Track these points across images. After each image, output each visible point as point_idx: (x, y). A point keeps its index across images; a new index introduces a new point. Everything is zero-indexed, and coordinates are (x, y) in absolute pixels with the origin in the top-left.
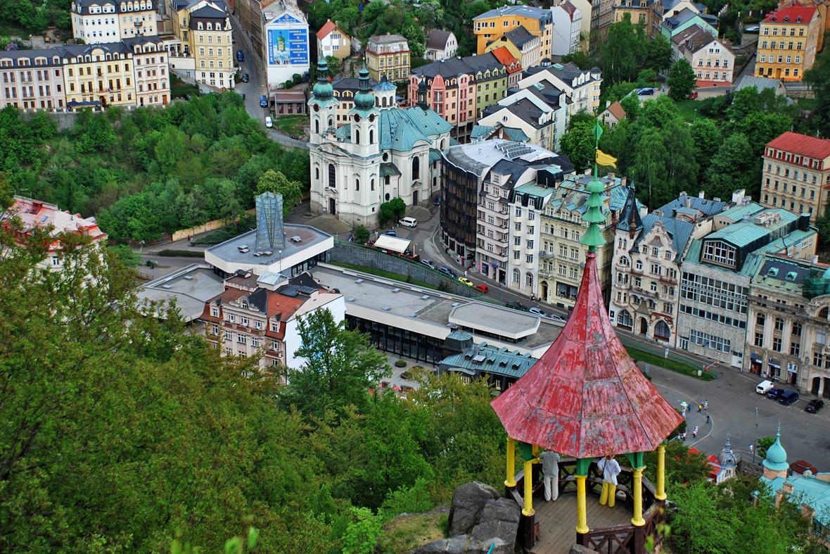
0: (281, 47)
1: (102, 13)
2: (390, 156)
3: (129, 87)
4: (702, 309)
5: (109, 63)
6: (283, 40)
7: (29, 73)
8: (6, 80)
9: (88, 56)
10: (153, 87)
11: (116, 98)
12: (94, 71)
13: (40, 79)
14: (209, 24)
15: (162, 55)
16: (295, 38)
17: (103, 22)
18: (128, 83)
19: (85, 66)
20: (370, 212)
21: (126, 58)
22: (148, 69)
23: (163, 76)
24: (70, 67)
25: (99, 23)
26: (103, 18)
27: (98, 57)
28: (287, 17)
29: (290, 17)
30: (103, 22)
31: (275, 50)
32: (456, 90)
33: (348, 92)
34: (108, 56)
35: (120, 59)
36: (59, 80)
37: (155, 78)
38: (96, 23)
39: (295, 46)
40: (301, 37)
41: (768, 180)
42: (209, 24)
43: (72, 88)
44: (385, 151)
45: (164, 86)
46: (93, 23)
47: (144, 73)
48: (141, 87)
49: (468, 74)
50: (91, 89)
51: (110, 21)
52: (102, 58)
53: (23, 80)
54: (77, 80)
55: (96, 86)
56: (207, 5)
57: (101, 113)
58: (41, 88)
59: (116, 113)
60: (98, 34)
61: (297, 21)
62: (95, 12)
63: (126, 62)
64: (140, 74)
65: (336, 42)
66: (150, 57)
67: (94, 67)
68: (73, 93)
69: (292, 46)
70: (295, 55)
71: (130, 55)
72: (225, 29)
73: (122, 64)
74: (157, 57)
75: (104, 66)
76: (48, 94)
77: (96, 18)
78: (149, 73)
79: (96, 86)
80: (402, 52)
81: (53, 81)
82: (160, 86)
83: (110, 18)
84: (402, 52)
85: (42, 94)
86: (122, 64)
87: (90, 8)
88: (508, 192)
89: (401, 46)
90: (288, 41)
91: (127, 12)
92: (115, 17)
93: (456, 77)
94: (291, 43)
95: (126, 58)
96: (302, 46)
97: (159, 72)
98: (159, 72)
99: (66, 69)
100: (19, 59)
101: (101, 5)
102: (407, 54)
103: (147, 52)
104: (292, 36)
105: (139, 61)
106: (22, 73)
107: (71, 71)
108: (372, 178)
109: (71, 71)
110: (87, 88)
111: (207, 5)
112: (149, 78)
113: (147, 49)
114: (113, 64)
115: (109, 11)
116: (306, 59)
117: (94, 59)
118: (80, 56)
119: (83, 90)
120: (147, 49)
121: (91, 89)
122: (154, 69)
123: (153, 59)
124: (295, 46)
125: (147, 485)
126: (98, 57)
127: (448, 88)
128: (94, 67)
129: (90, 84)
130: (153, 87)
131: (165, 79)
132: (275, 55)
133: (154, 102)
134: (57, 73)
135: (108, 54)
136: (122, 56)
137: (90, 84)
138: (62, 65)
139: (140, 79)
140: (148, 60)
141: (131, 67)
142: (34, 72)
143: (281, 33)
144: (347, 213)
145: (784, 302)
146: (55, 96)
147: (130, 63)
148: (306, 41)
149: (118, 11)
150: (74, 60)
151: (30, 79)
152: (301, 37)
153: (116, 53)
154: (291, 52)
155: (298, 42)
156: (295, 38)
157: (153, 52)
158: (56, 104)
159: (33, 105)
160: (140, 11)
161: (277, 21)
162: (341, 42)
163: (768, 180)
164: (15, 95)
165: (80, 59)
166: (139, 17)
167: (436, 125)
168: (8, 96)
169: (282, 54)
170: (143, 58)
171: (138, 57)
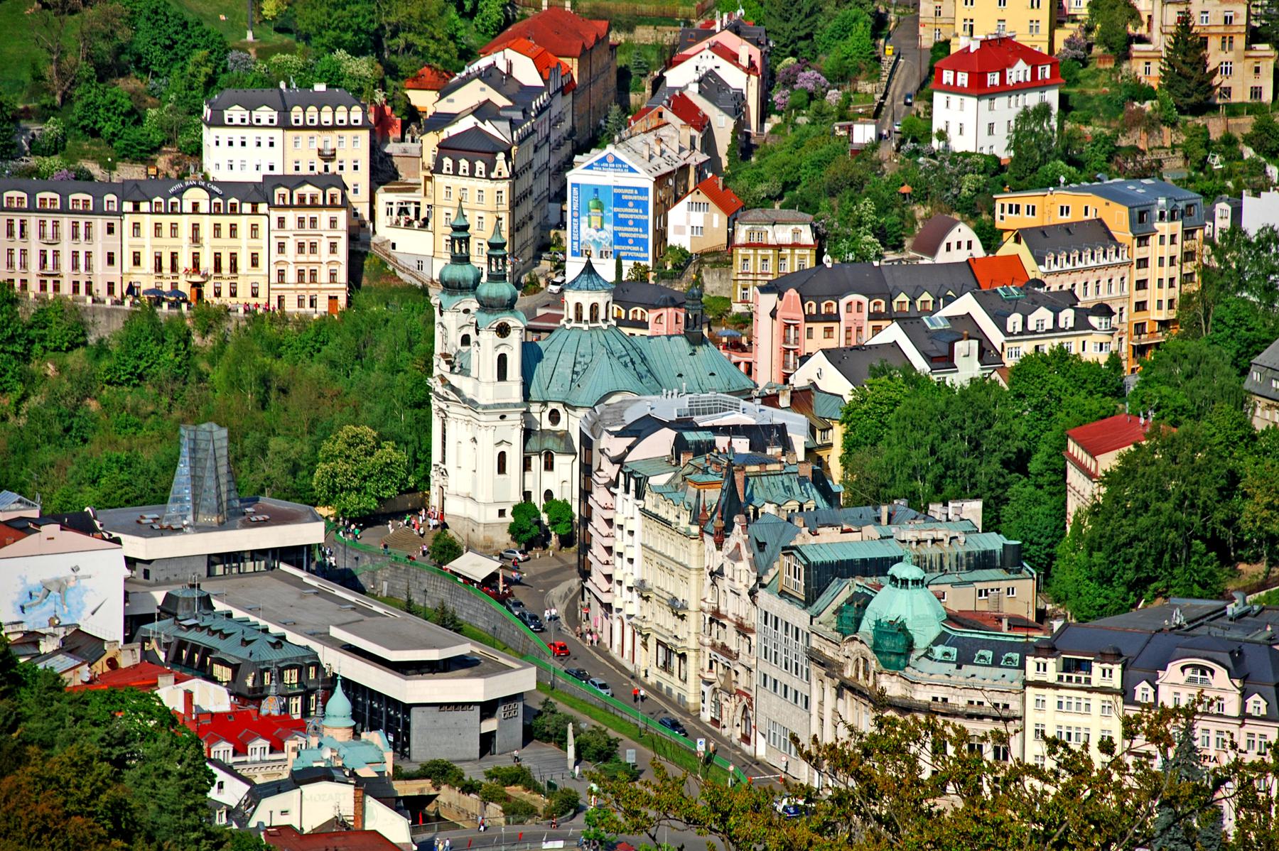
0: (596, 221)
1: (251, 126)
2: (563, 416)
3: (254, 271)
5: (217, 219)
6: (600, 206)
7: (56, 224)
8: (10, 234)
9: (174, 199)
10: (307, 277)
11: (225, 292)
13: (75, 236)
14: (464, 164)
15: (333, 213)
16: (624, 204)
17: (251, 143)
18: (255, 263)
19: (166, 220)
20: (493, 516)
21: (255, 211)
22: (301, 239)
23: (333, 257)
24: (136, 218)
25: (243, 144)
26: (251, 135)
27: (195, 206)
28: (610, 159)
29: (617, 161)
30: (251, 143)
31: (584, 226)
32: (835, 325)
33: (639, 309)
34: (217, 205)
35: (241, 214)
36: (112, 243)
37: (313, 258)
38: (237, 143)
39: (623, 222)
40: (638, 204)
41: (502, 375)
42: (464, 164)
43: (137, 261)
44: (552, 406)
45: (333, 275)
46: (231, 144)
47: (291, 247)
48: (281, 274)
49: (870, 296)
50: (174, 268)
51: (265, 143)
52: (204, 207)
53: (42, 235)
54: (148, 245)
55: (185, 262)
56: (476, 127)
57: (181, 314)
58: (75, 255)
59: (212, 318)
60: (236, 165)
61: (631, 170)
62: (237, 121)
63: (254, 219)
64: (281, 247)
65: (698, 218)
66: (307, 214)
67: (185, 223)
68: (136, 270)
69: (619, 222)
70: (623, 241)
71: (263, 208)
72: (494, 175)
74: (324, 217)
75: (206, 224)
76: (88, 267)
77: (236, 134)
78: (301, 246)
79: (185, 262)
80: (794, 246)
81: (101, 244)
82: (323, 276)
83: (265, 135)
84: (794, 246)
85: (75, 266)
86: (243, 223)
87: (226, 113)
89: (709, 220)
90: (610, 211)
91: (305, 128)
92: (277, 134)
93: (837, 296)
94: (616, 214)
95: (255, 211)
96: (637, 223)
97: (324, 247)
98: (324, 247)
99: (129, 220)
100: (39, 196)
101: (251, 107)
102: (807, 251)
103: (302, 205)
104: (619, 201)
105: (281, 221)
106: (42, 224)
107: (136, 226)
108: (503, 448)
109: (136, 226)
110: (166, 263)
111: (476, 127)
112: (302, 258)
113: (302, 198)
114: (225, 221)
115: (265, 121)
116: (646, 251)
117: (187, 207)
118: (158, 199)
119: (159, 267)
120: (302, 198)
121: (174, 268)
122: (313, 239)
123: (313, 220)
124: (623, 222)
126: (195, 206)
127: (809, 318)
128: (185, 223)
129: (174, 256)
130: (307, 277)
131: (337, 262)
132: (584, 237)
133: (307, 308)
134: (110, 230)
135: (217, 200)
136: (247, 208)
137: (174, 256)
138: (120, 213)
139: (281, 257)
140: (301, 220)
142: (66, 222)
143: (596, 191)
144: (458, 517)
145: (945, 700)
146: (102, 274)
147: (262, 222)
148: (646, 212)
149: (285, 125)
150: (144, 206)
151: (56, 235)
152: (638, 204)
153: (233, 200)
154: (615, 233)
155: (629, 213)
156: (624, 204)
157: (313, 206)
158: (100, 288)
159: (56, 287)
160: (334, 127)
161: (590, 167)
162: (709, 220)
163: (502, 375)
164: (24, 265)
165: (158, 204)
166: (331, 139)
167: (705, 375)
168: (10, 265)
169: (596, 235)
170: (291, 217)
171: (282, 213)
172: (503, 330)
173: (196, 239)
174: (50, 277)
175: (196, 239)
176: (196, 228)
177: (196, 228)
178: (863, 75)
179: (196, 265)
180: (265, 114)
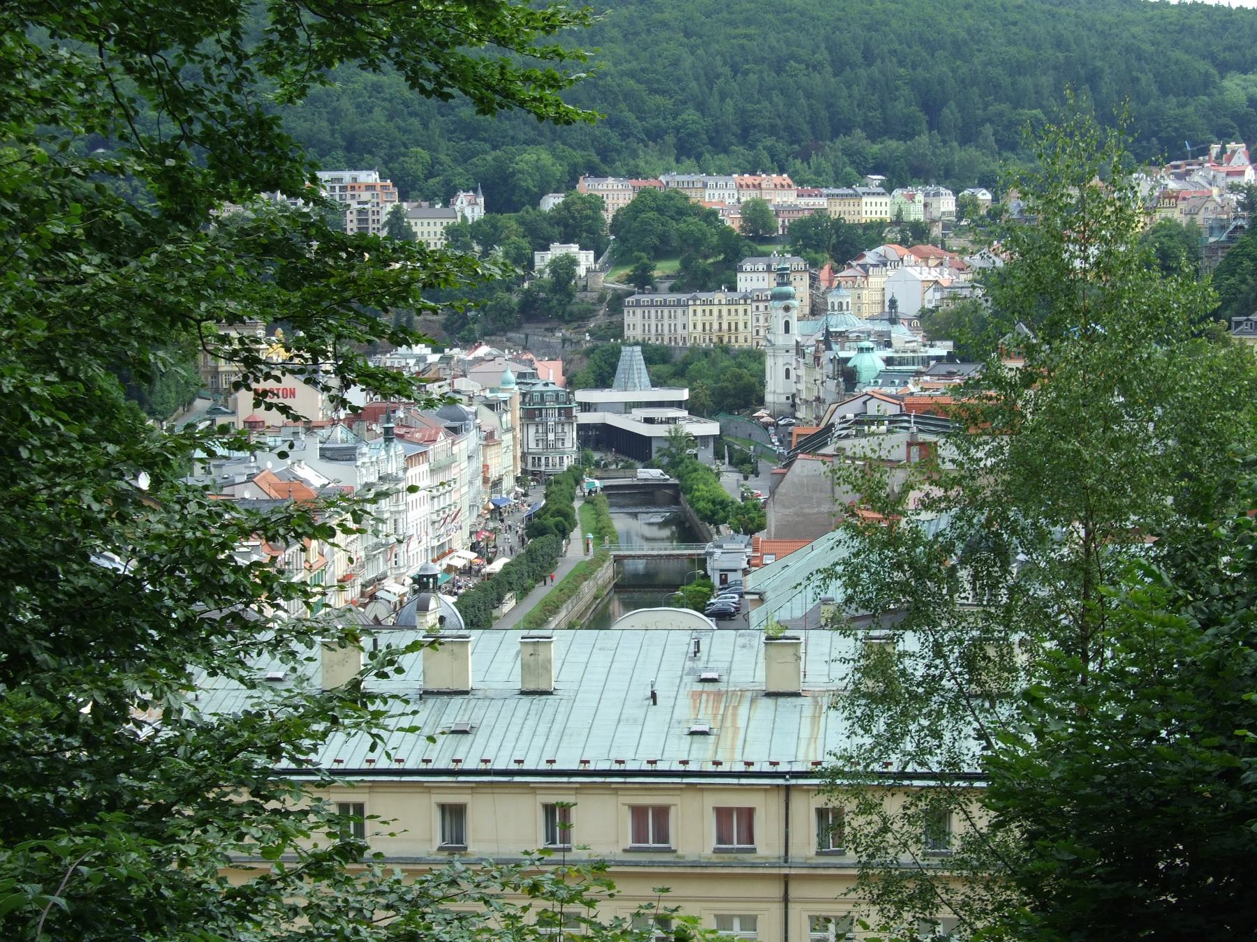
4: (806, 924)
12: (716, 313)
17: (755, 278)
19: (707, 308)
26: (755, 276)
30: (755, 278)
36: (428, 229)
59: (726, 350)
73: (741, 309)
79: (716, 326)
81: (680, 320)
83: (761, 276)
86: (741, 309)
88: (10, 192)
92: (766, 275)
99: (691, 309)
105: (757, 307)
114: (733, 308)
117: (716, 302)
125: (1070, 391)
128: (715, 310)
141: (749, 312)
147: (749, 308)
172: (787, 309)
173: (720, 316)
174: (659, 335)
175: (720, 316)
176: (720, 311)
177: (720, 311)
178: (987, 310)
179: (720, 329)
180: (761, 266)
